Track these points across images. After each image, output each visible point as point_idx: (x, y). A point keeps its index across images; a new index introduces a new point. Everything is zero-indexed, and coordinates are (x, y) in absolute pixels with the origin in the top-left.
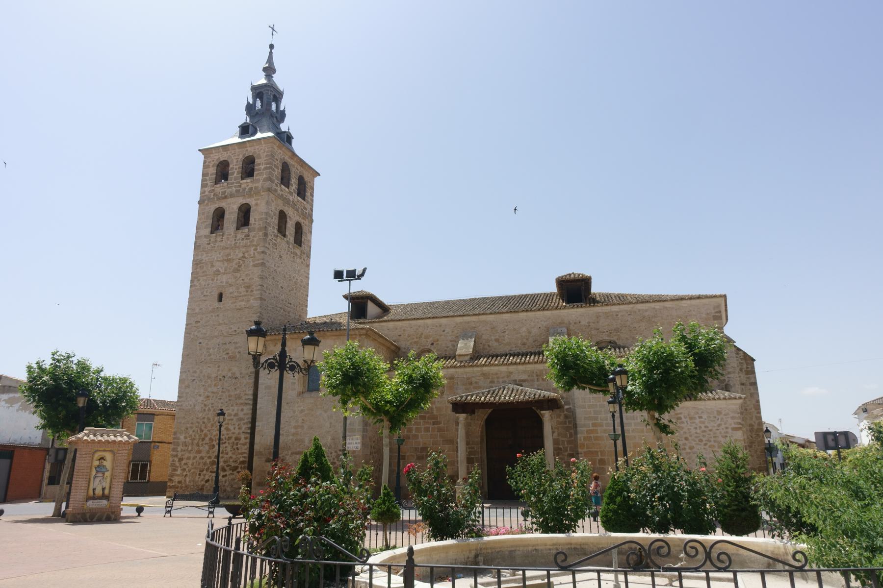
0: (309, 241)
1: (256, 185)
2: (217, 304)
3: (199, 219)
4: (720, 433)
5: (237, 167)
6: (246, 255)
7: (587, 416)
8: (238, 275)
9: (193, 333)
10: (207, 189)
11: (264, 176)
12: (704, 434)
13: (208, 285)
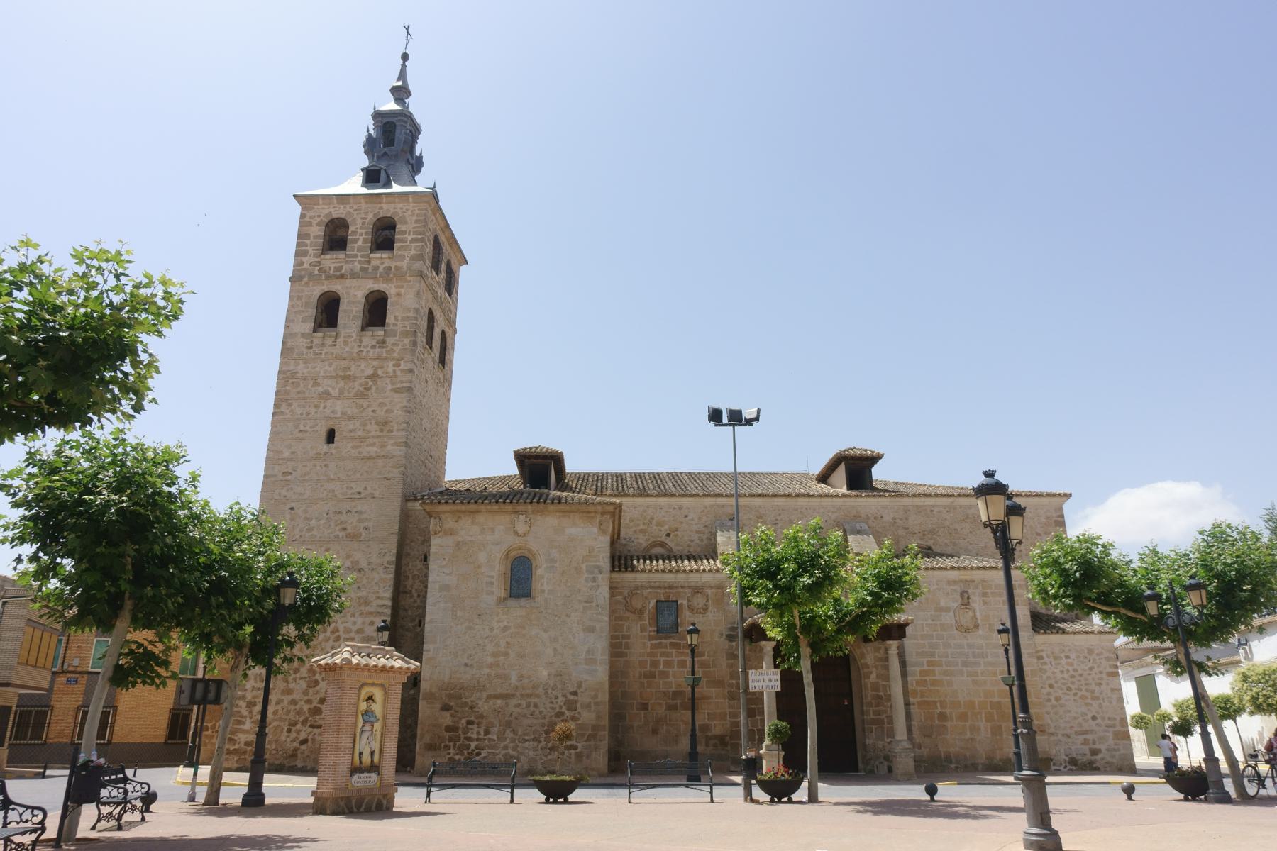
0: (451, 362)
1: (399, 264)
2: (325, 447)
3: (291, 306)
4: (1093, 679)
5: (364, 231)
6: (380, 372)
8: (365, 403)
9: (277, 492)
10: (307, 260)
11: (413, 252)
12: (1073, 680)
13: (308, 414)
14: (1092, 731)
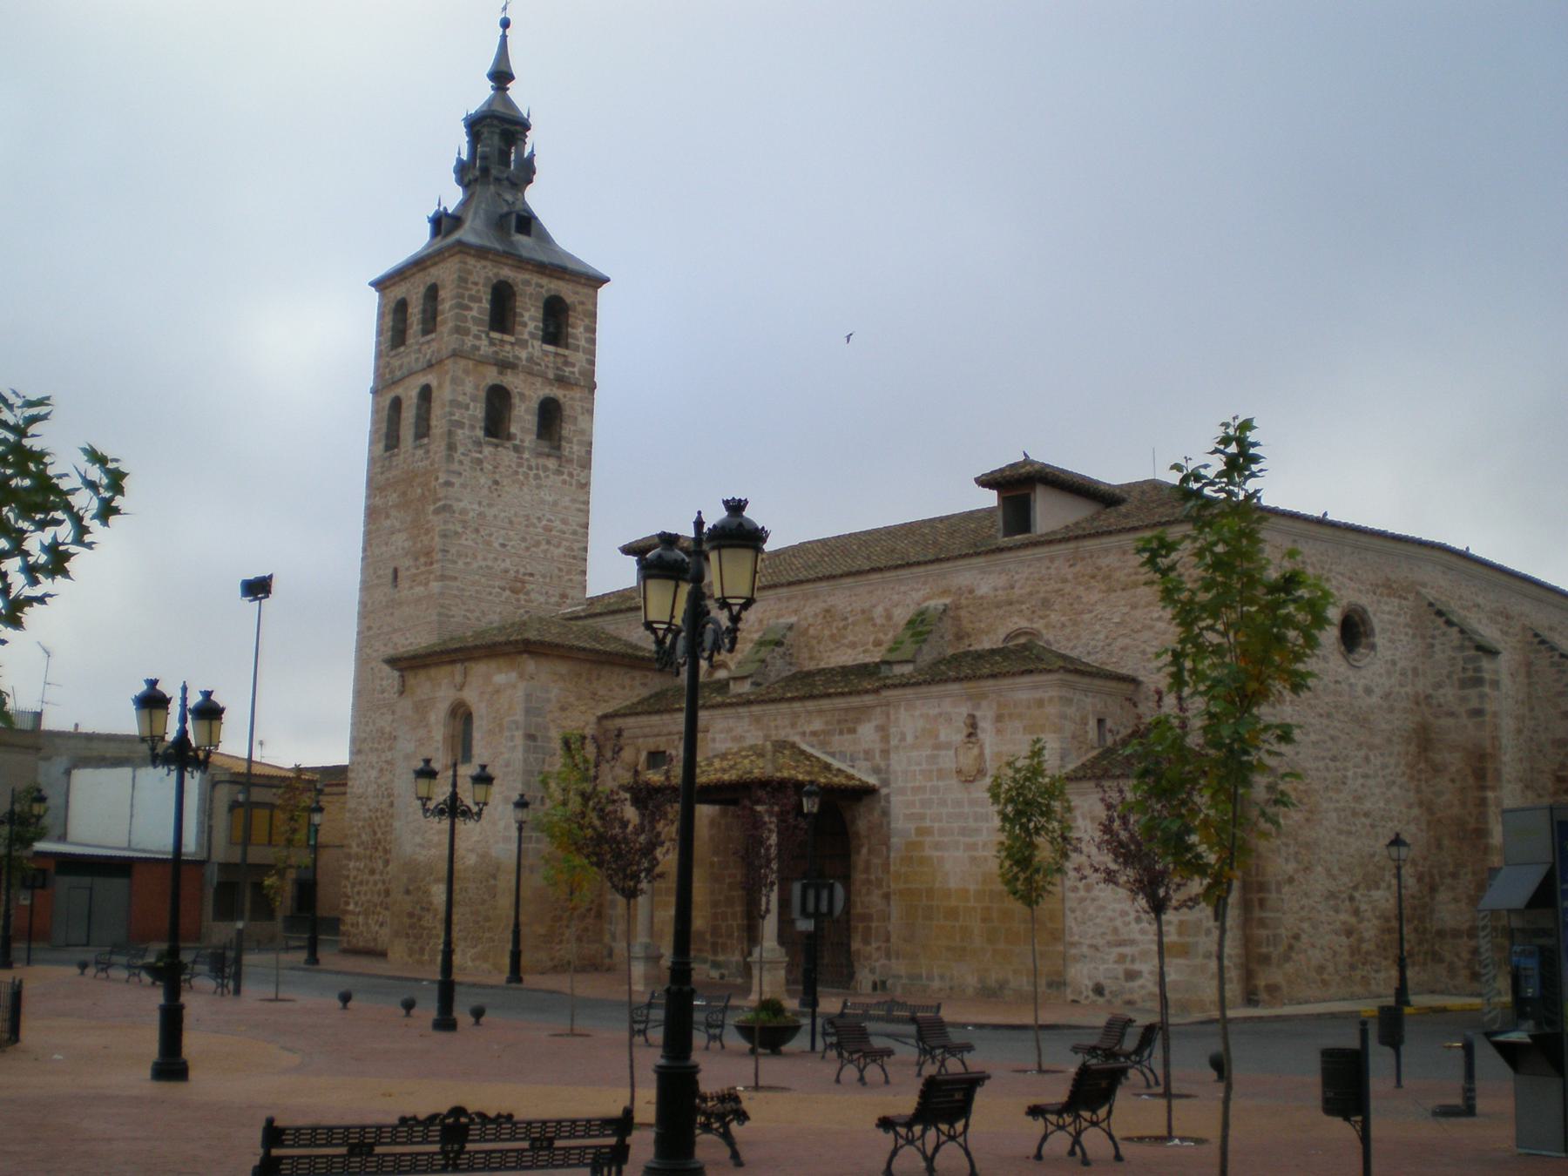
7: (908, 812)
14: (1132, 942)
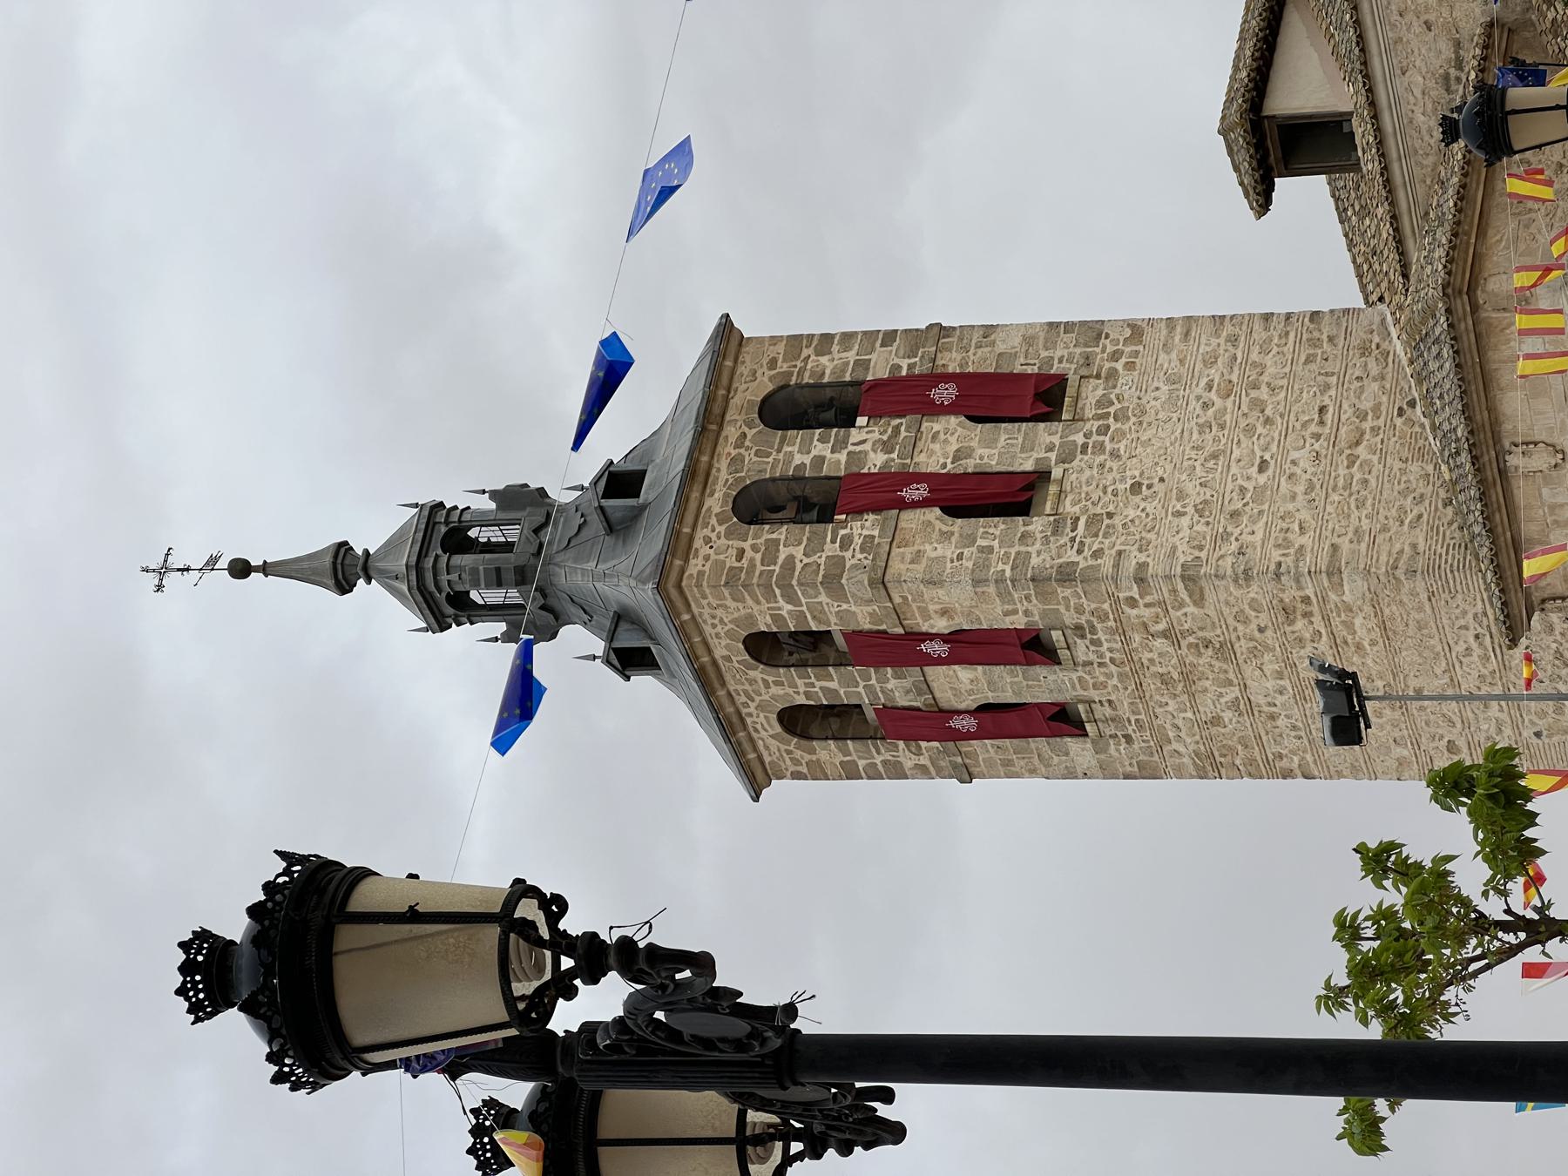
5: (800, 682)
8: (1242, 647)
11: (823, 598)
13: (1294, 728)
